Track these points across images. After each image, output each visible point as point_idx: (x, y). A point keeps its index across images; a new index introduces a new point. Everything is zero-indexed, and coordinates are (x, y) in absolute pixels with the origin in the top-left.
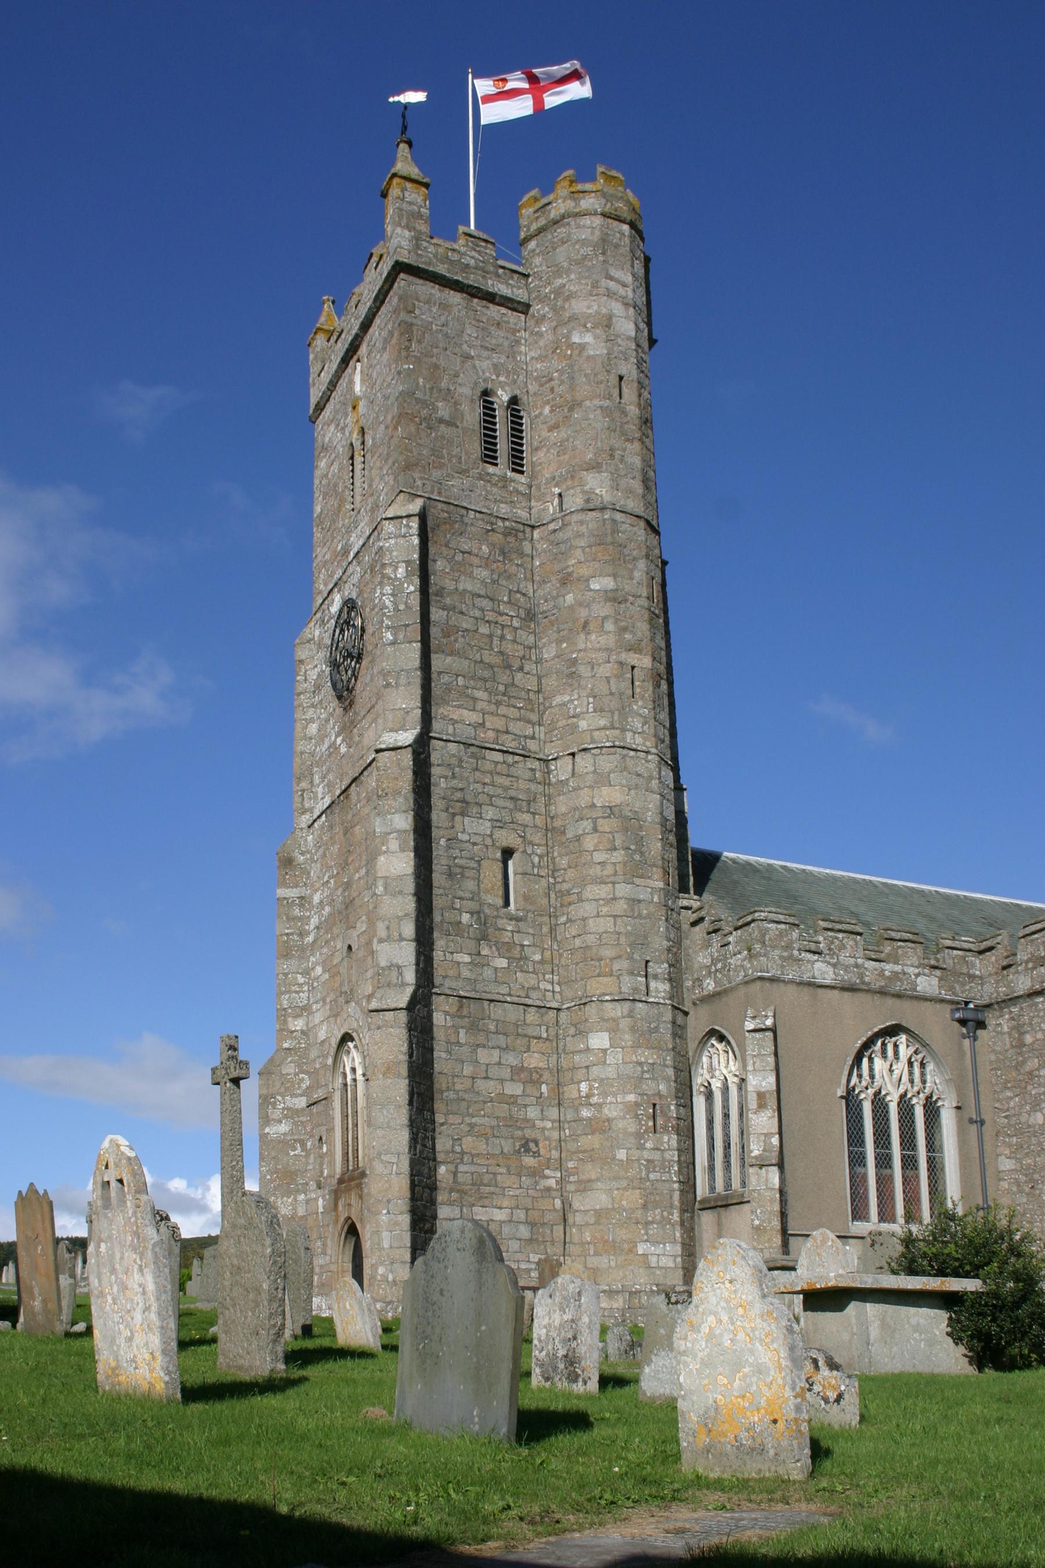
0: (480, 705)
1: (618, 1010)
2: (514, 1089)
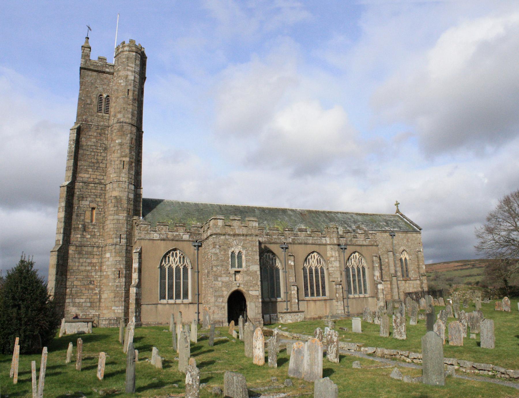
0: (90, 173)
1: (111, 248)
2: (89, 268)
